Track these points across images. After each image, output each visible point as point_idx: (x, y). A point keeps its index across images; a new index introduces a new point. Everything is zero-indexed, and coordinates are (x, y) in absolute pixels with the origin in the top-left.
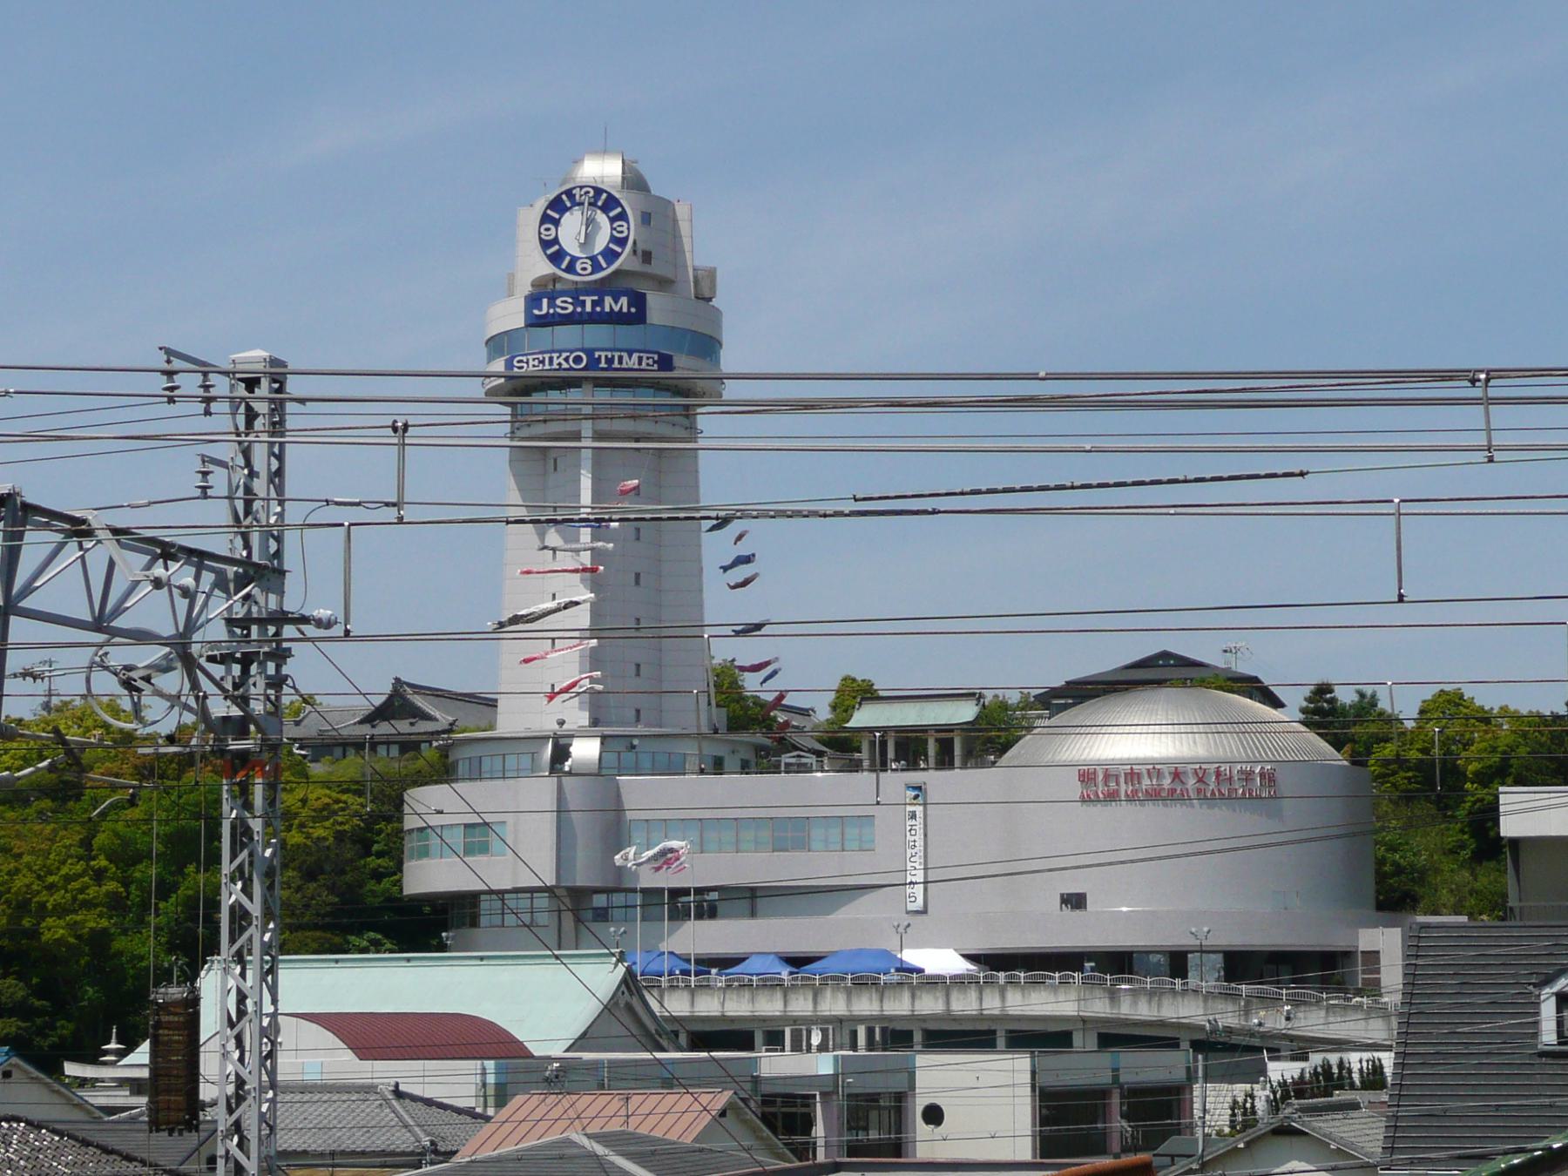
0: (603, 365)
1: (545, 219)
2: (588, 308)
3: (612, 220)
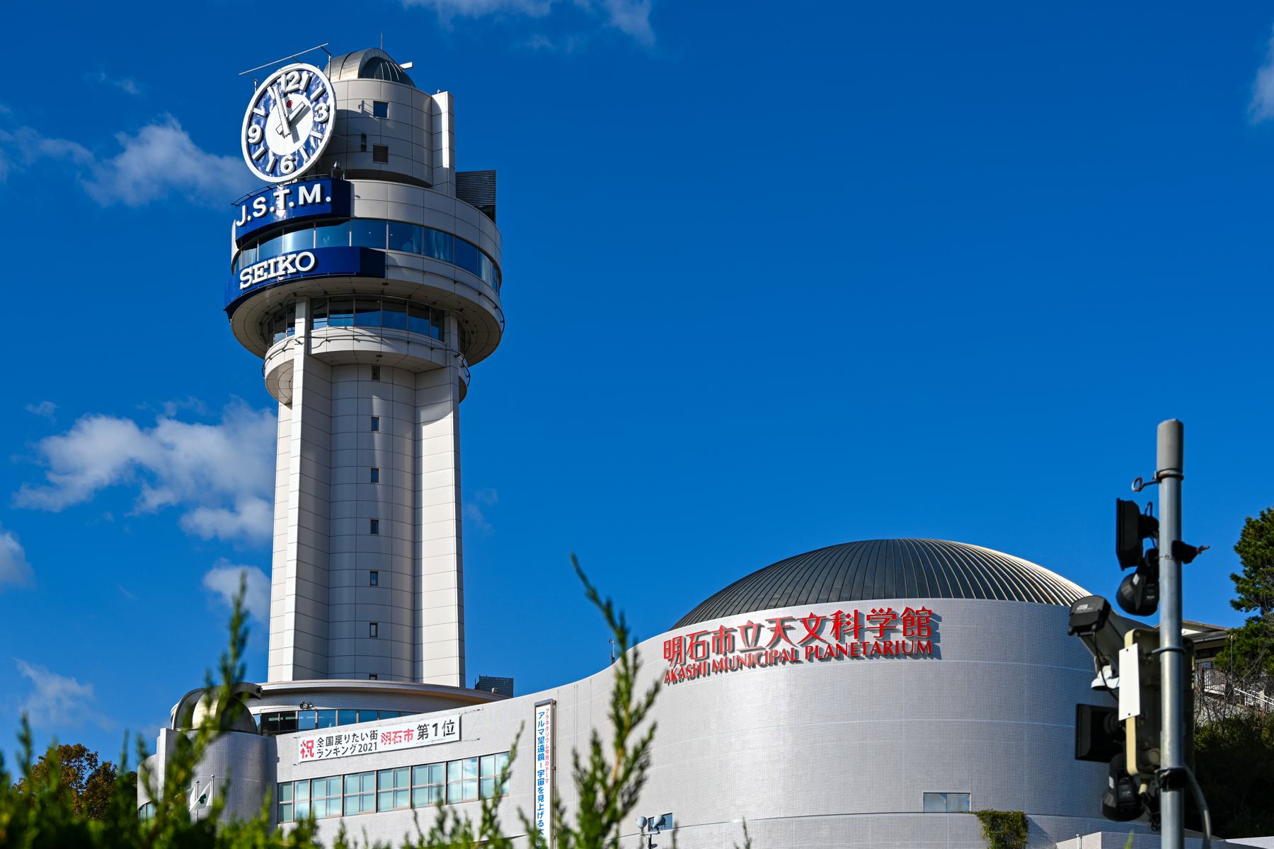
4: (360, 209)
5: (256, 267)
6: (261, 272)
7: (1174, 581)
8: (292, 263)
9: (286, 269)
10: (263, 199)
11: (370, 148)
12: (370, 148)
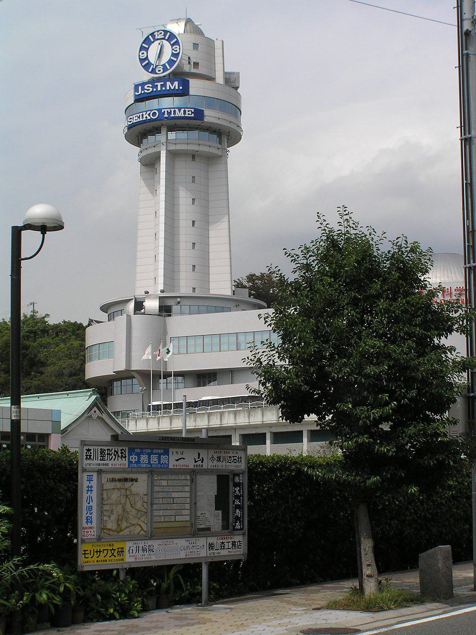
0: (166, 115)
1: (142, 48)
2: (159, 89)
3: (172, 45)
4: (192, 91)
5: (134, 116)
6: (136, 118)
7: (467, 412)
8: (149, 115)
9: (146, 117)
10: (150, 85)
11: (192, 63)
12: (192, 63)
